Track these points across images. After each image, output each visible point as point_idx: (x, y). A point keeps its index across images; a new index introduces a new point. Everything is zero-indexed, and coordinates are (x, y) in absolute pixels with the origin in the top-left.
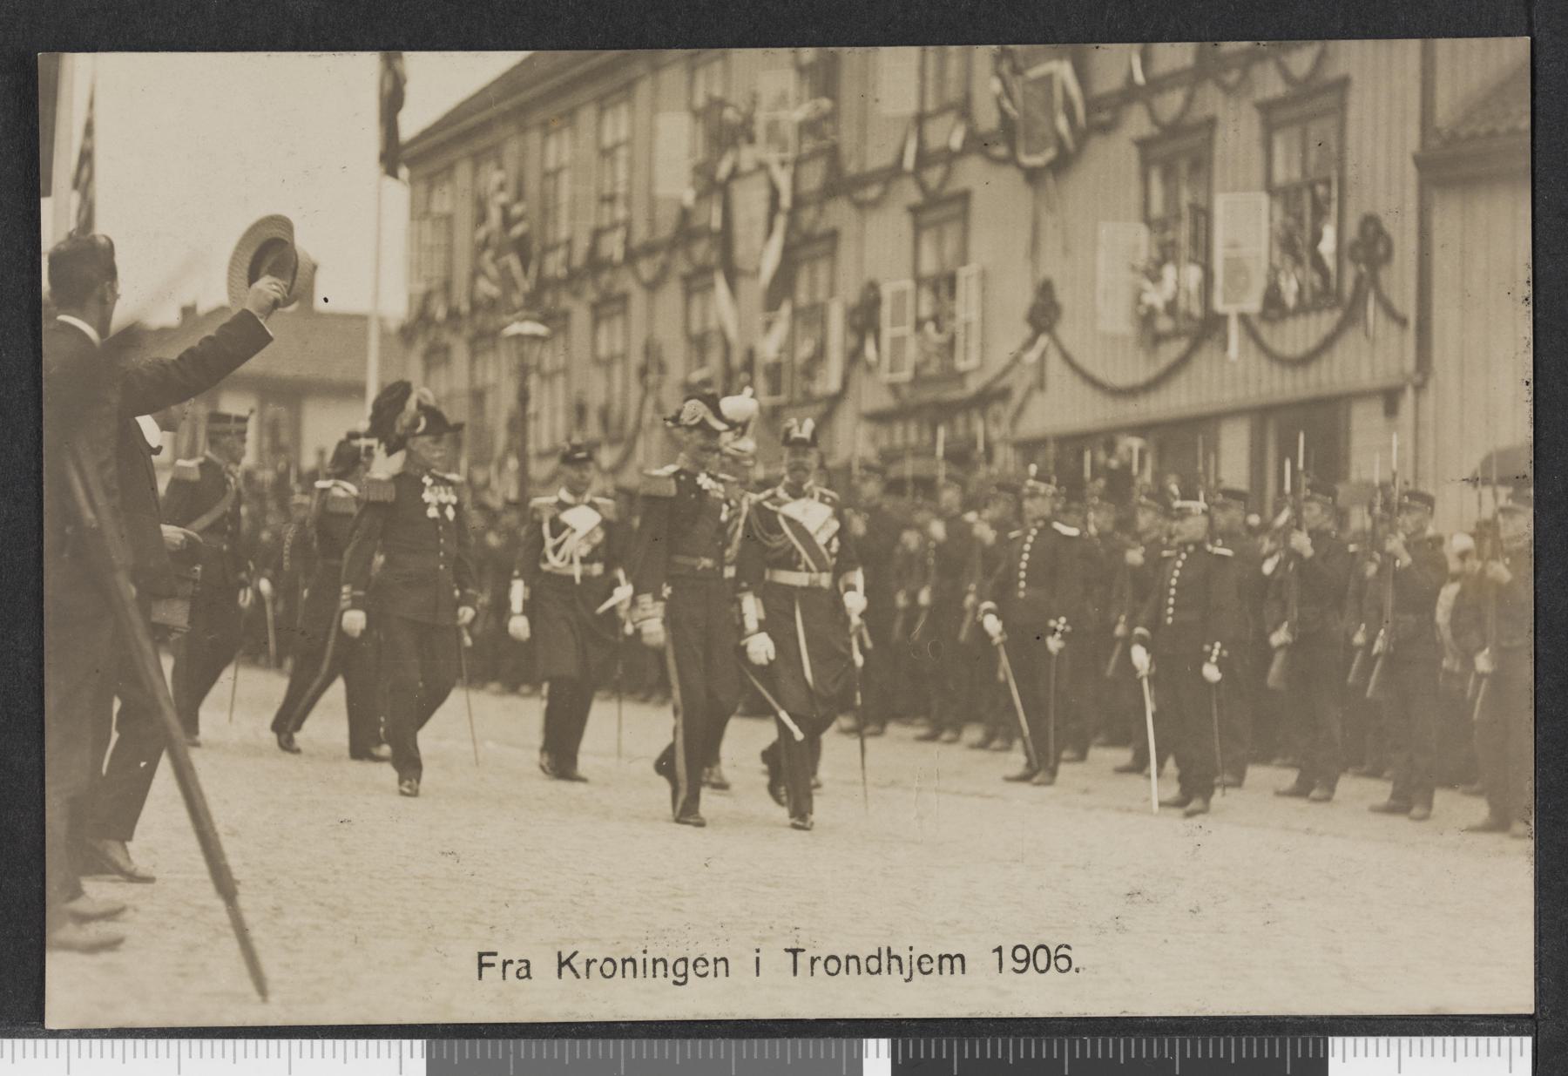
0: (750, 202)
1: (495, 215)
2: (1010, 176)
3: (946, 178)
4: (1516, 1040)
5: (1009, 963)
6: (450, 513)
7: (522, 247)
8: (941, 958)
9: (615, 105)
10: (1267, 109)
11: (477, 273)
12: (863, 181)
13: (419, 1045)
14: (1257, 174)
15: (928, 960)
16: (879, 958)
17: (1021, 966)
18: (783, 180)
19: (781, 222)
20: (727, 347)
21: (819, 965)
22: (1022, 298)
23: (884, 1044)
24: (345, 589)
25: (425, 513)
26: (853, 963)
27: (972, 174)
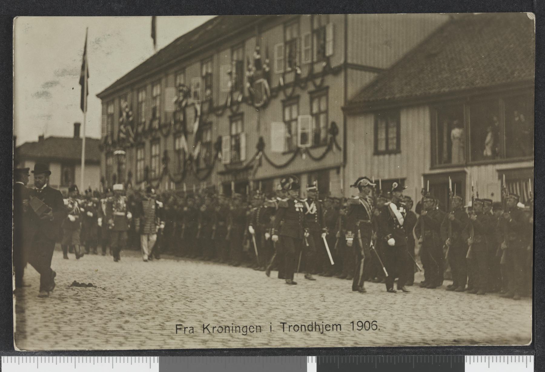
0: (190, 113)
1: (124, 114)
2: (252, 108)
3: (238, 109)
4: (528, 357)
5: (356, 327)
6: (301, 210)
7: (132, 124)
8: (333, 325)
9: (157, 85)
10: (311, 93)
11: (120, 131)
12: (218, 108)
13: (156, 358)
14: (308, 110)
15: (252, 328)
16: (312, 325)
17: (360, 328)
18: (198, 107)
19: (198, 119)
20: (185, 153)
21: (291, 328)
22: (256, 141)
23: (314, 358)
24: (273, 229)
25: (295, 210)
26: (303, 327)
27: (244, 108)
